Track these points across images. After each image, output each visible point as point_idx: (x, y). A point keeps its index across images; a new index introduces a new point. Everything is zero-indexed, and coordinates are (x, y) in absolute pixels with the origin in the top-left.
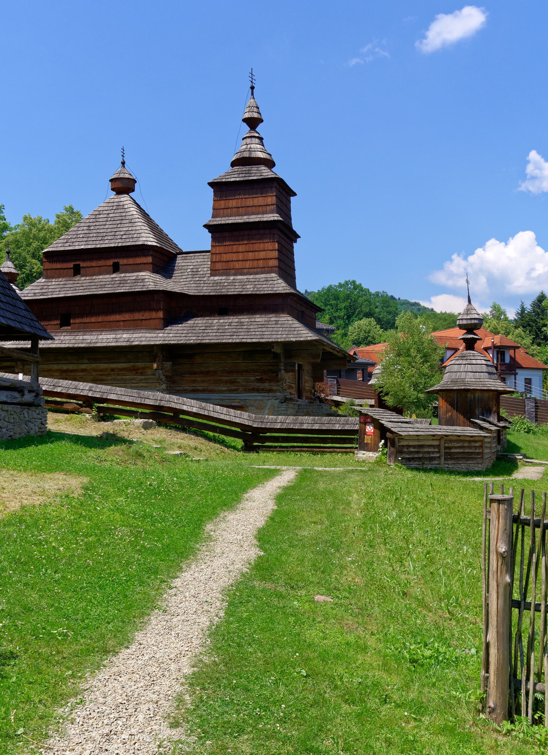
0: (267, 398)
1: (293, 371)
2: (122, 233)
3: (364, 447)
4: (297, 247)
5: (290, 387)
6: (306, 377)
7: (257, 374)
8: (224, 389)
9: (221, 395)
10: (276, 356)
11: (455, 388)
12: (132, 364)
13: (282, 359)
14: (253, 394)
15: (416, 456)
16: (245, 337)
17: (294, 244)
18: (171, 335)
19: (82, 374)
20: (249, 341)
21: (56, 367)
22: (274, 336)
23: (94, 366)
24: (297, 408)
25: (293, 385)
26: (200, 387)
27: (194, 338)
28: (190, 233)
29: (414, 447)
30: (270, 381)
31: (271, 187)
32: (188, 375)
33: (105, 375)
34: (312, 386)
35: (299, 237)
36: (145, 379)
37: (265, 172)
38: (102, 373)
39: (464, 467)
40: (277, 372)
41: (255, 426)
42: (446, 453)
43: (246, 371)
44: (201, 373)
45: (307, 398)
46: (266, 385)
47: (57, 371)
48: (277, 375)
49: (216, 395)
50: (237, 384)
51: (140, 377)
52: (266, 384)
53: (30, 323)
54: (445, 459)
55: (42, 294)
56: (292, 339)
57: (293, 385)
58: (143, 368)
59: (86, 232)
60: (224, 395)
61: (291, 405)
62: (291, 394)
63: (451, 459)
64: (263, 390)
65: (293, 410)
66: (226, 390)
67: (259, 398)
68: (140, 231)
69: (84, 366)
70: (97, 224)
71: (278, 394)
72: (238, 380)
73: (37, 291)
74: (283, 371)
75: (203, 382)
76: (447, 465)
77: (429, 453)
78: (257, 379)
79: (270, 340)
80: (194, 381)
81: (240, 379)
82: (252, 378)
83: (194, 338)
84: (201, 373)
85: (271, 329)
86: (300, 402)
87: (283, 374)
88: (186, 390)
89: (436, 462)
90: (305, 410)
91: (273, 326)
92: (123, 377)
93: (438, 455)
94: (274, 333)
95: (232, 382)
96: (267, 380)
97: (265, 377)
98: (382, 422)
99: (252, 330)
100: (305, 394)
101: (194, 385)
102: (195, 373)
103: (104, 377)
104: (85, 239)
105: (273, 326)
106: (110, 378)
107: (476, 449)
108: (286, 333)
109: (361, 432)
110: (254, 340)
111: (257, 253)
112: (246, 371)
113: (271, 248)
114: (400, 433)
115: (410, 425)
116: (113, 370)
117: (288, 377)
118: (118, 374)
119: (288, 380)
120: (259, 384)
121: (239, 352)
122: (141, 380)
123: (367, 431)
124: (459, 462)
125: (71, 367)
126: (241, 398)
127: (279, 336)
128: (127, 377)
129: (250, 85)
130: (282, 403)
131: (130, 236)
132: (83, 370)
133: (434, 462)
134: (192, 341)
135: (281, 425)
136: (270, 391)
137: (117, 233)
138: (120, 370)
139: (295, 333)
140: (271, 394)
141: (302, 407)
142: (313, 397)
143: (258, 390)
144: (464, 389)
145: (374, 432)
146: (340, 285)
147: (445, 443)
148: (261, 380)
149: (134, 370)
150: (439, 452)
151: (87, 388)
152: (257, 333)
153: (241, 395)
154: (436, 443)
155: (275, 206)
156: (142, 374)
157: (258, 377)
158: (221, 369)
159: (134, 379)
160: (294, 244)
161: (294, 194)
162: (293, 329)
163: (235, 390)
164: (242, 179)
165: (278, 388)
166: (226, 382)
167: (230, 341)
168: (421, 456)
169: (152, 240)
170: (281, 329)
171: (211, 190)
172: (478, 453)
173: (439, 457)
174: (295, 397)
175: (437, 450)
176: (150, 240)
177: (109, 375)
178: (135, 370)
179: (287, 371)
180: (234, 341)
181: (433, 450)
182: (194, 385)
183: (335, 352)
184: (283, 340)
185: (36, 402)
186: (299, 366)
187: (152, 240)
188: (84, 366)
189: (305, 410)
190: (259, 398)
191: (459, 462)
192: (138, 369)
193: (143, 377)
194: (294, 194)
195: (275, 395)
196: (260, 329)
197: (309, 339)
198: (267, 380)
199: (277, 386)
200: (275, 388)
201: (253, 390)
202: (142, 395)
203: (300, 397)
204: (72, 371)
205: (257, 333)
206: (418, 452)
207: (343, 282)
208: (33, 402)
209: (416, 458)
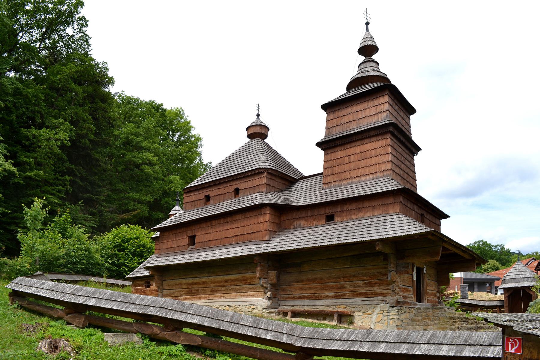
0: (376, 303)
4: (420, 161)
6: (428, 281)
7: (365, 278)
8: (331, 294)
9: (326, 301)
17: (415, 157)
19: (203, 286)
20: (350, 241)
21: (184, 281)
23: (212, 278)
26: (306, 293)
28: (308, 160)
30: (380, 284)
31: (383, 96)
32: (296, 284)
33: (221, 286)
34: (436, 290)
35: (419, 149)
36: (253, 288)
38: (218, 284)
43: (354, 276)
44: (309, 280)
46: (376, 289)
47: (185, 284)
49: (322, 301)
50: (344, 290)
51: (248, 286)
52: (375, 288)
57: (411, 289)
58: (251, 278)
61: (404, 309)
64: (372, 294)
66: (332, 296)
69: (204, 279)
72: (346, 285)
75: (310, 289)
78: (366, 284)
80: (301, 289)
81: (347, 284)
82: (360, 283)
84: (309, 280)
86: (419, 305)
88: (294, 297)
90: (424, 314)
92: (235, 287)
95: (339, 288)
96: (376, 283)
97: (374, 281)
100: (426, 298)
101: (301, 292)
102: (302, 281)
103: (219, 288)
106: (224, 288)
110: (355, 240)
111: (368, 160)
113: (383, 153)
116: (226, 281)
120: (367, 289)
121: (347, 256)
125: (195, 280)
126: (348, 304)
128: (238, 287)
130: (393, 307)
132: (204, 283)
135: (371, 347)
136: (379, 295)
138: (232, 281)
140: (380, 298)
141: (422, 311)
142: (437, 300)
143: (366, 295)
148: (370, 284)
149: (244, 280)
152: (361, 233)
153: (348, 300)
155: (388, 112)
156: (250, 284)
158: (327, 276)
160: (415, 157)
163: (342, 296)
165: (389, 291)
166: (333, 288)
174: (414, 300)
177: (223, 286)
182: (301, 292)
183: (461, 254)
188: (204, 279)
190: (367, 303)
192: (247, 279)
193: (251, 286)
194: (446, 216)
195: (385, 299)
199: (388, 289)
200: (385, 291)
201: (361, 295)
204: (195, 284)
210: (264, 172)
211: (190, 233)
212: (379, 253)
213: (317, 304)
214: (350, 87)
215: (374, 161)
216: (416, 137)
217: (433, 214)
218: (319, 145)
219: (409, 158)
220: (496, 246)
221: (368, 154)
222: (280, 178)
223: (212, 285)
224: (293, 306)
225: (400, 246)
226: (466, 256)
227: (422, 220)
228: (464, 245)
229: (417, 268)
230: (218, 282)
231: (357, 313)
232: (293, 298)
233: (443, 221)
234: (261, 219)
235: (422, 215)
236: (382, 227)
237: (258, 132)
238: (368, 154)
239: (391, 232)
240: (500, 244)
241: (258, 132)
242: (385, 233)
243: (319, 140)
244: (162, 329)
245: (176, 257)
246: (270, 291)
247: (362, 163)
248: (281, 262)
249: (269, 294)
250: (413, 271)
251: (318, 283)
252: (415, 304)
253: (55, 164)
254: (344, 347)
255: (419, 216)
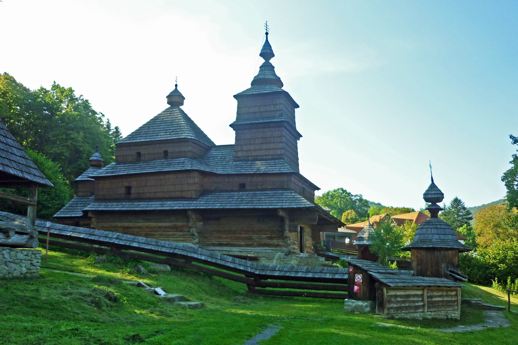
1: (296, 231)
2: (171, 131)
3: (353, 296)
5: (294, 244)
6: (307, 237)
8: (243, 243)
10: (282, 219)
11: (425, 246)
12: (174, 223)
13: (287, 222)
14: (264, 248)
15: (403, 305)
16: (258, 204)
17: (298, 141)
18: (202, 203)
19: (137, 230)
20: (260, 207)
21: (119, 224)
22: (280, 204)
23: (147, 224)
24: (299, 259)
25: (296, 242)
27: (219, 205)
29: (401, 296)
33: (155, 231)
36: (183, 235)
37: (275, 89)
39: (443, 314)
40: (282, 231)
41: (257, 273)
42: (428, 302)
43: (260, 231)
45: (307, 252)
46: (275, 242)
48: (283, 234)
53: (11, 163)
54: (428, 308)
55: (112, 173)
56: (293, 206)
57: (296, 242)
58: (182, 227)
59: (147, 130)
60: (243, 248)
62: (294, 249)
63: (433, 307)
65: (295, 261)
66: (243, 245)
67: (269, 251)
68: (184, 130)
69: (140, 224)
70: (155, 125)
71: (284, 249)
73: (109, 171)
74: (287, 231)
75: (227, 238)
76: (430, 313)
77: (414, 302)
78: (268, 237)
79: (277, 207)
80: (220, 238)
81: (255, 236)
82: (264, 236)
83: (219, 205)
85: (278, 199)
86: (302, 255)
87: (287, 233)
89: (421, 310)
91: (280, 196)
93: (422, 304)
94: (280, 202)
95: (250, 239)
96: (275, 237)
98: (371, 273)
99: (263, 199)
100: (306, 250)
104: (145, 135)
105: (280, 196)
106: (158, 233)
107: (452, 298)
108: (289, 201)
109: (351, 282)
110: (264, 207)
112: (260, 231)
114: (389, 284)
115: (396, 277)
116: (160, 227)
117: (293, 237)
118: (164, 231)
119: (291, 238)
122: (180, 235)
123: (356, 280)
124: (440, 310)
125: (130, 224)
127: (283, 204)
128: (171, 233)
129: (265, 31)
131: (176, 133)
132: (139, 227)
133: (419, 311)
134: (216, 207)
136: (277, 246)
137: (168, 131)
139: (297, 201)
140: (278, 248)
144: (432, 247)
145: (363, 282)
146: (335, 191)
147: (427, 293)
148: (270, 238)
150: (423, 301)
151: (115, 237)
152: (267, 202)
154: (420, 293)
157: (268, 235)
159: (175, 234)
161: (298, 106)
162: (295, 199)
164: (258, 93)
167: (246, 207)
168: (407, 305)
169: (192, 135)
170: (285, 199)
171: (235, 102)
172: (454, 301)
173: (423, 306)
174: (298, 251)
175: (420, 299)
176: (189, 135)
178: (176, 228)
179: (290, 231)
180: (249, 207)
181: (417, 299)
184: (286, 207)
185: (29, 244)
186: (301, 228)
187: (192, 135)
189: (305, 261)
190: (269, 251)
191: (440, 310)
192: (179, 227)
193: (181, 233)
194: (298, 106)
196: (269, 199)
197: (307, 206)
198: (275, 237)
200: (281, 243)
201: (265, 245)
202: (159, 244)
203: (302, 251)
205: (267, 202)
206: (404, 302)
207: (336, 189)
208: (25, 244)
209: (403, 307)
211: (126, 184)
213: (233, 250)
215: (272, 146)
218: (231, 126)
220: (355, 196)
223: (147, 230)
224: (228, 251)
226: (332, 220)
230: (152, 228)
231: (262, 258)
232: (213, 245)
234: (191, 181)
236: (281, 199)
237: (175, 99)
239: (288, 204)
240: (358, 194)
241: (175, 99)
242: (283, 204)
243: (231, 122)
244: (326, 260)
245: (115, 204)
246: (197, 238)
248: (206, 215)
249: (197, 240)
251: (233, 234)
252: (299, 254)
254: (282, 274)
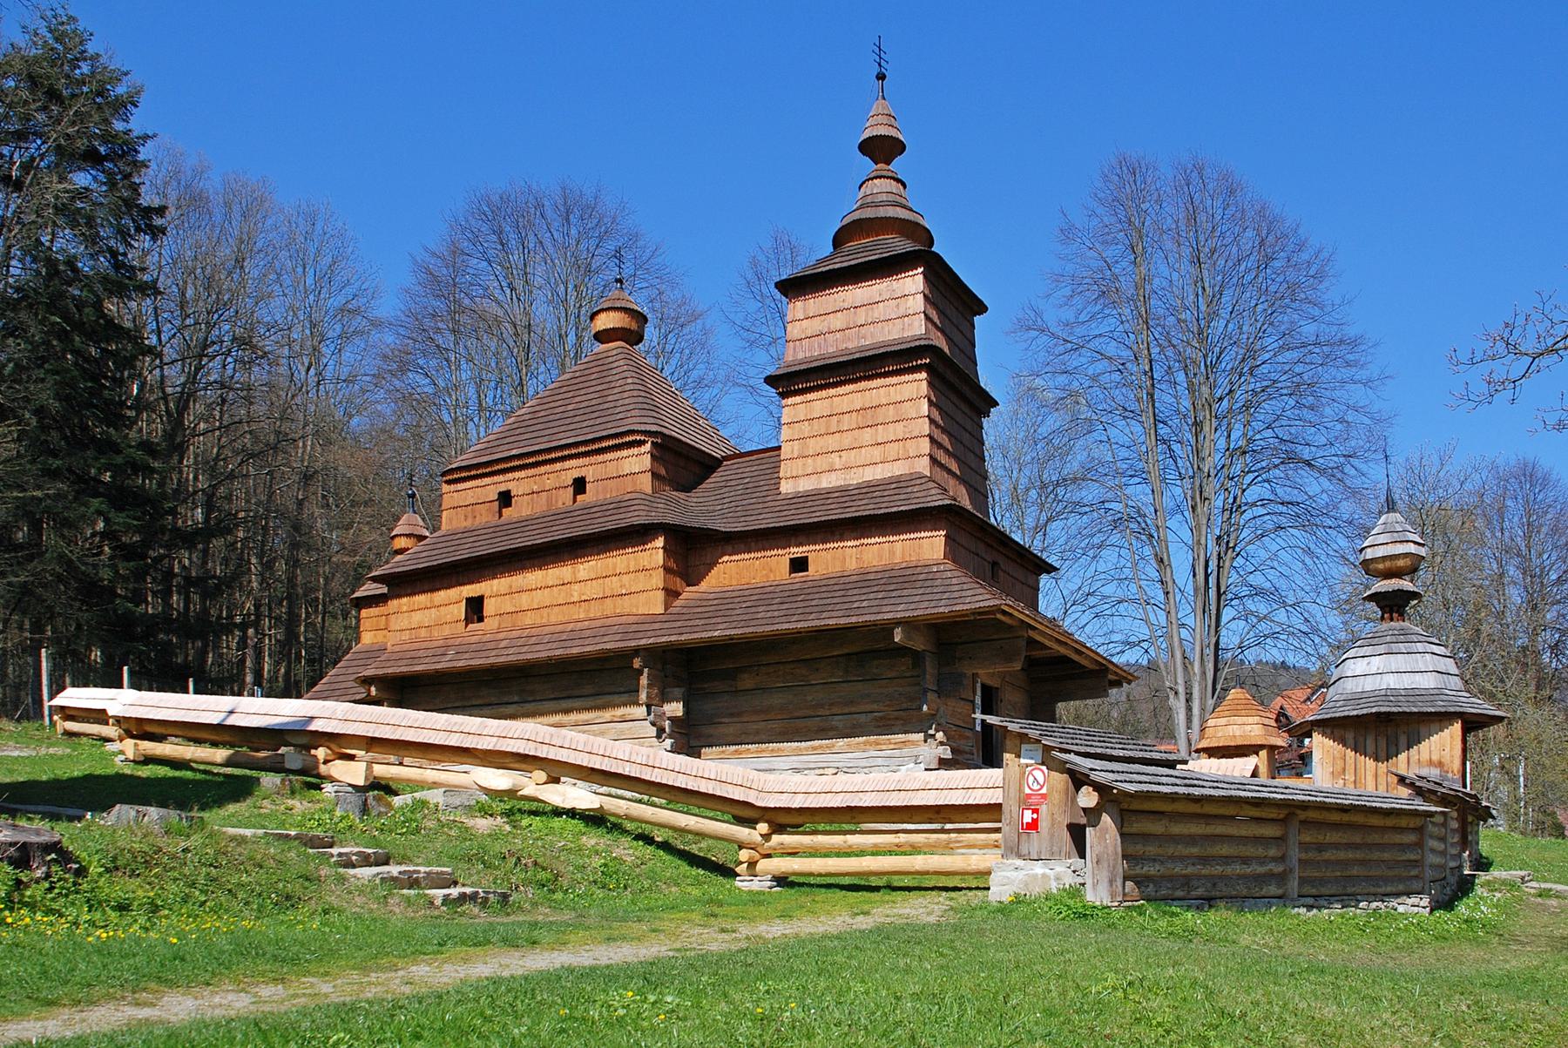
17: (985, 421)
160: (985, 421)
210: (644, 442)
212: (901, 650)
214: (839, 240)
216: (985, 381)
217: (1020, 566)
219: (969, 425)
221: (881, 415)
222: (679, 454)
225: (951, 638)
227: (990, 575)
228: (215, 722)
229: (983, 686)
233: (1044, 580)
235: (994, 564)
238: (881, 415)
247: (867, 436)
250: (974, 693)
253: (129, 362)
255: (988, 567)
